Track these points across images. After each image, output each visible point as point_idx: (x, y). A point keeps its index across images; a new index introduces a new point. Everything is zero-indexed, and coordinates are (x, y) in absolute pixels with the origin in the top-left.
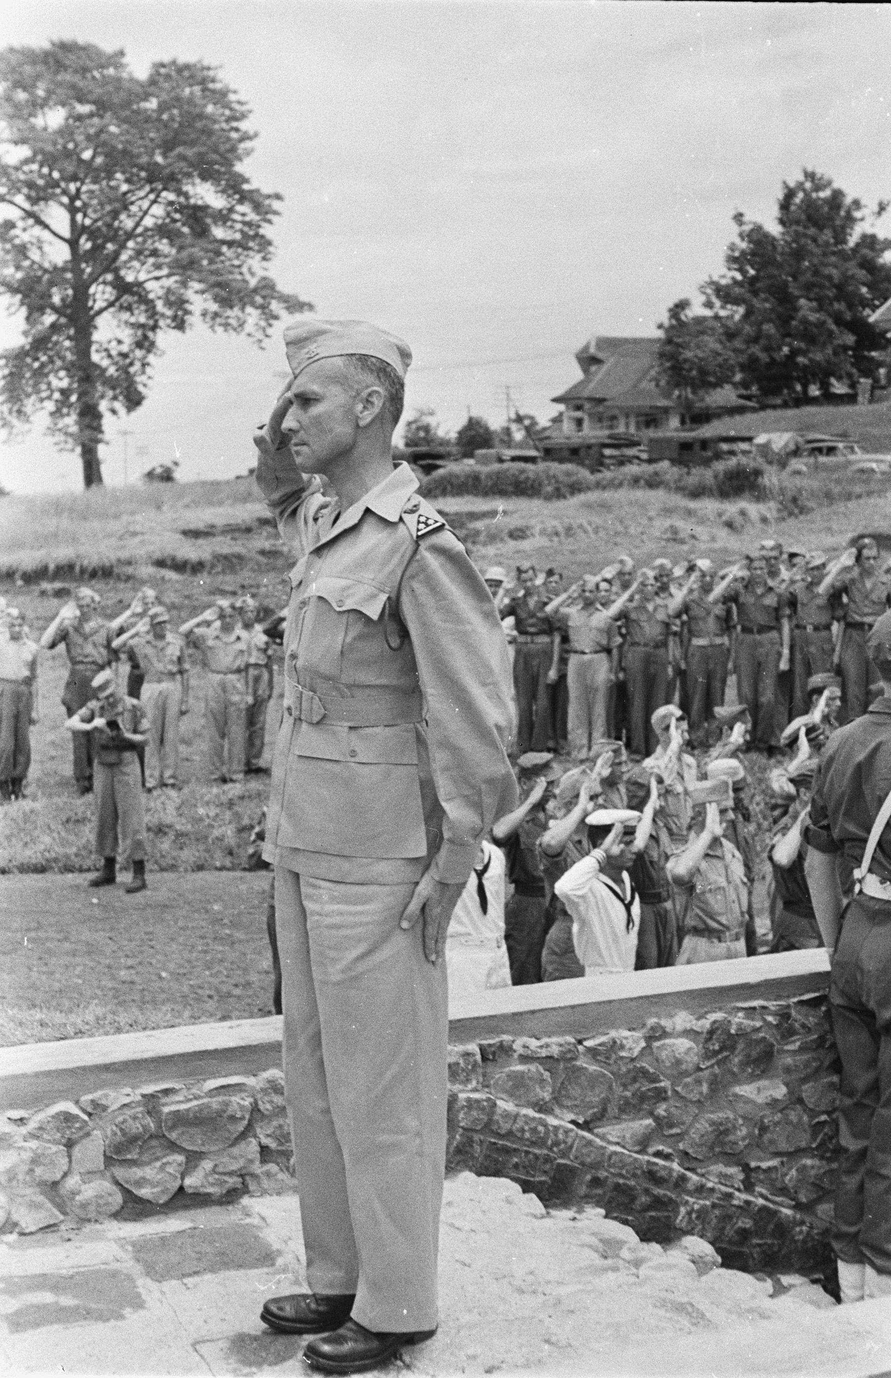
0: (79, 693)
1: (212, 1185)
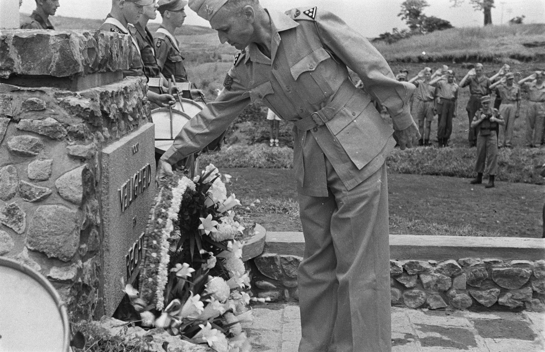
0: (474, 106)
1: (510, 303)
